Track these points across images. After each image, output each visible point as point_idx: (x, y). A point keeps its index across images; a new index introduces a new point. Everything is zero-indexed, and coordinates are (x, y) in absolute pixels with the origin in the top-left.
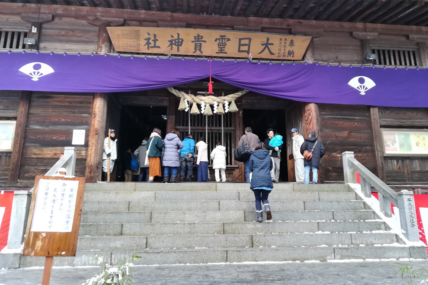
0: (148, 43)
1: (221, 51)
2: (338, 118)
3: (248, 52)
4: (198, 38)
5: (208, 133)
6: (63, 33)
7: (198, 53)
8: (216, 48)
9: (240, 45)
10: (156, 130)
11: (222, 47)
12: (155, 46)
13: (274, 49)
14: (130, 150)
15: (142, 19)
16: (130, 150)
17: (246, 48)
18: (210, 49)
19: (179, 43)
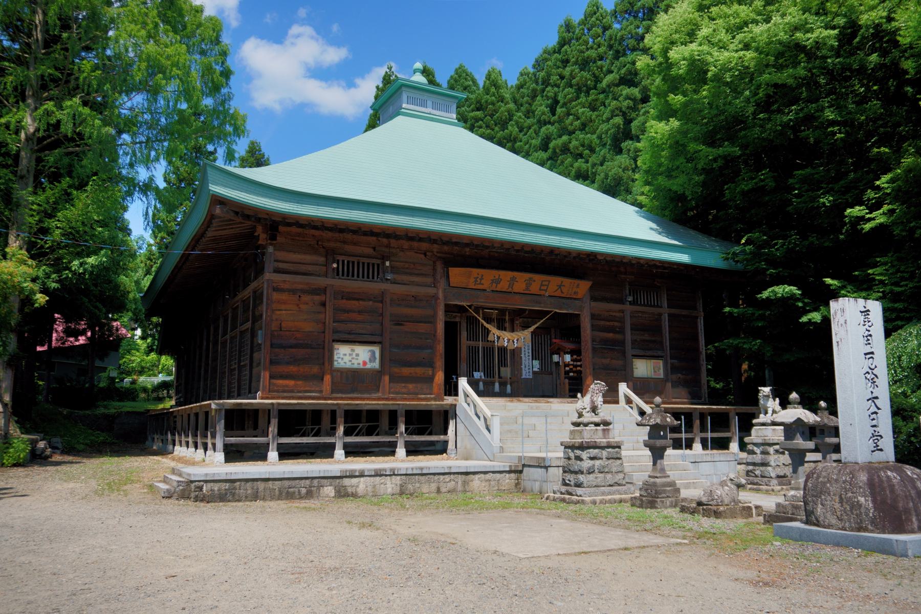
0: (476, 281)
1: (527, 289)
2: (603, 320)
3: (546, 290)
4: (513, 279)
5: (692, 404)
6: (407, 266)
7: (510, 290)
8: (524, 286)
9: (542, 285)
10: (377, 350)
11: (528, 286)
12: (480, 284)
13: (565, 290)
14: (788, 209)
15: (465, 241)
16: (788, 209)
17: (545, 288)
18: (519, 287)
19: (498, 281)
